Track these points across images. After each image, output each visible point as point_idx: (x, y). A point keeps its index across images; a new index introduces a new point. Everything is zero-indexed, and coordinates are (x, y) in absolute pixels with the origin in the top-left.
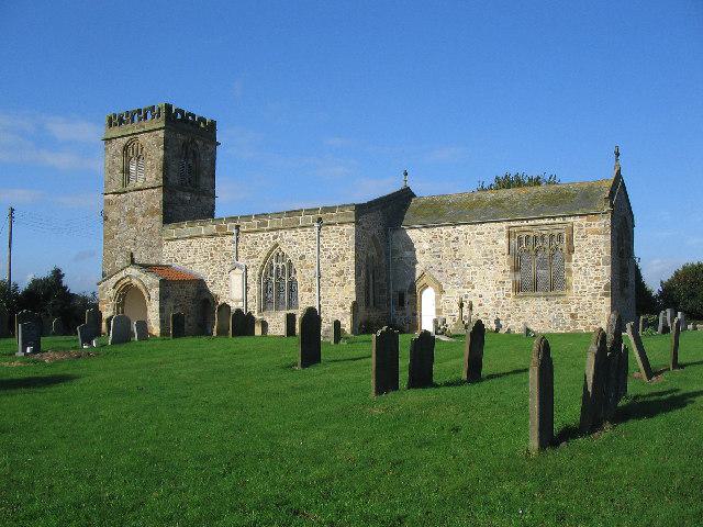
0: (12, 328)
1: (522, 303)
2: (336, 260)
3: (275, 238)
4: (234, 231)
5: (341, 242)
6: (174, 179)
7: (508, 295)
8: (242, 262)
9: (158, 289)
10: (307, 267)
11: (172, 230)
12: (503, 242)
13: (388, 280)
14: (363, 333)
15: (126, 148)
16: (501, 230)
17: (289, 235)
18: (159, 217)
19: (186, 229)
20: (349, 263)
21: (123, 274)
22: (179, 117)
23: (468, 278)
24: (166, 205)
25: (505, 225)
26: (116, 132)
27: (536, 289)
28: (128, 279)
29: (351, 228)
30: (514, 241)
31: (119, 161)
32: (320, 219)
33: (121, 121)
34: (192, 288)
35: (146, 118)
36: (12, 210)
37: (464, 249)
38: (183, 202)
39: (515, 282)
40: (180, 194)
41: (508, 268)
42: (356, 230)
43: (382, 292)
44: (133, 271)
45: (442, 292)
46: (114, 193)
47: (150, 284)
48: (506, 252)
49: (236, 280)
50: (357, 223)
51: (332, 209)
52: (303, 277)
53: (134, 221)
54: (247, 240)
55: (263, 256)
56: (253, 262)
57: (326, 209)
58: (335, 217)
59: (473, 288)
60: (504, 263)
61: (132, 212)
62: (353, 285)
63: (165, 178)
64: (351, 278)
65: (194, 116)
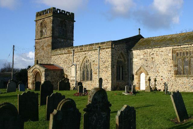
0: (17, 87)
1: (178, 79)
2: (105, 62)
3: (85, 54)
4: (73, 52)
5: (106, 55)
6: (57, 34)
7: (172, 76)
8: (75, 63)
9: (44, 73)
10: (96, 65)
11: (55, 52)
12: (170, 55)
13: (128, 70)
14: (120, 90)
15: (41, 24)
16: (170, 50)
17: (90, 53)
18: (50, 47)
19: (59, 51)
20: (109, 63)
21: (34, 68)
22: (58, 12)
23: (157, 69)
24: (53, 43)
25: (171, 48)
26: (39, 18)
27: (184, 74)
28: (36, 69)
29: (110, 50)
30: (174, 55)
31: (39, 28)
32: (100, 47)
33: (40, 15)
34: (59, 72)
35: (47, 13)
36: (14, 46)
37: (156, 58)
38: (60, 42)
39: (175, 71)
40: (59, 39)
41: (172, 65)
42: (112, 51)
43: (126, 74)
44: (37, 66)
45: (148, 74)
46: (38, 39)
47: (42, 70)
48: (172, 59)
49: (73, 69)
50: (112, 48)
51: (104, 43)
52: (94, 68)
53: (43, 49)
54: (77, 55)
55: (81, 61)
56: (78, 63)
57: (102, 43)
58: (104, 46)
59: (159, 73)
60: (171, 63)
61: (43, 46)
62: (110, 72)
63: (53, 33)
64: (110, 69)
65: (64, 11)
